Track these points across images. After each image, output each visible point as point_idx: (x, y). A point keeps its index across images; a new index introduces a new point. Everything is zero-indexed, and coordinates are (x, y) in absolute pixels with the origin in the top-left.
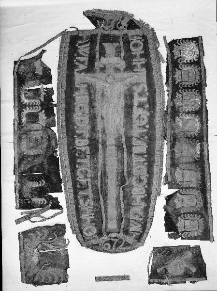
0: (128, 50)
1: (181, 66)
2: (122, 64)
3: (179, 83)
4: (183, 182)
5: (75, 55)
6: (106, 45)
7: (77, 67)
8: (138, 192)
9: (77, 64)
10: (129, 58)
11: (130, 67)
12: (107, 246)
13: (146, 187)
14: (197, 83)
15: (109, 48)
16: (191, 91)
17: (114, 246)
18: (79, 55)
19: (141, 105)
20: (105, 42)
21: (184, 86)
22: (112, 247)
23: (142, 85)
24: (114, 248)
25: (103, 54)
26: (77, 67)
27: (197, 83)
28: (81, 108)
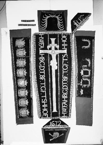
0: (61, 41)
1: (26, 106)
2: (58, 47)
3: (27, 100)
4: (23, 61)
5: (39, 43)
6: (51, 39)
7: (40, 47)
8: (65, 96)
9: (66, 104)
10: (61, 44)
11: (61, 48)
12: (53, 125)
13: (67, 94)
14: (20, 100)
15: (53, 40)
16: (21, 96)
17: (56, 124)
18: (65, 108)
19: (65, 62)
20: (56, 112)
21: (25, 99)
22: (55, 124)
23: (65, 54)
24: (56, 125)
25: (50, 42)
26: (40, 47)
27: (20, 100)
28: (15, 33)
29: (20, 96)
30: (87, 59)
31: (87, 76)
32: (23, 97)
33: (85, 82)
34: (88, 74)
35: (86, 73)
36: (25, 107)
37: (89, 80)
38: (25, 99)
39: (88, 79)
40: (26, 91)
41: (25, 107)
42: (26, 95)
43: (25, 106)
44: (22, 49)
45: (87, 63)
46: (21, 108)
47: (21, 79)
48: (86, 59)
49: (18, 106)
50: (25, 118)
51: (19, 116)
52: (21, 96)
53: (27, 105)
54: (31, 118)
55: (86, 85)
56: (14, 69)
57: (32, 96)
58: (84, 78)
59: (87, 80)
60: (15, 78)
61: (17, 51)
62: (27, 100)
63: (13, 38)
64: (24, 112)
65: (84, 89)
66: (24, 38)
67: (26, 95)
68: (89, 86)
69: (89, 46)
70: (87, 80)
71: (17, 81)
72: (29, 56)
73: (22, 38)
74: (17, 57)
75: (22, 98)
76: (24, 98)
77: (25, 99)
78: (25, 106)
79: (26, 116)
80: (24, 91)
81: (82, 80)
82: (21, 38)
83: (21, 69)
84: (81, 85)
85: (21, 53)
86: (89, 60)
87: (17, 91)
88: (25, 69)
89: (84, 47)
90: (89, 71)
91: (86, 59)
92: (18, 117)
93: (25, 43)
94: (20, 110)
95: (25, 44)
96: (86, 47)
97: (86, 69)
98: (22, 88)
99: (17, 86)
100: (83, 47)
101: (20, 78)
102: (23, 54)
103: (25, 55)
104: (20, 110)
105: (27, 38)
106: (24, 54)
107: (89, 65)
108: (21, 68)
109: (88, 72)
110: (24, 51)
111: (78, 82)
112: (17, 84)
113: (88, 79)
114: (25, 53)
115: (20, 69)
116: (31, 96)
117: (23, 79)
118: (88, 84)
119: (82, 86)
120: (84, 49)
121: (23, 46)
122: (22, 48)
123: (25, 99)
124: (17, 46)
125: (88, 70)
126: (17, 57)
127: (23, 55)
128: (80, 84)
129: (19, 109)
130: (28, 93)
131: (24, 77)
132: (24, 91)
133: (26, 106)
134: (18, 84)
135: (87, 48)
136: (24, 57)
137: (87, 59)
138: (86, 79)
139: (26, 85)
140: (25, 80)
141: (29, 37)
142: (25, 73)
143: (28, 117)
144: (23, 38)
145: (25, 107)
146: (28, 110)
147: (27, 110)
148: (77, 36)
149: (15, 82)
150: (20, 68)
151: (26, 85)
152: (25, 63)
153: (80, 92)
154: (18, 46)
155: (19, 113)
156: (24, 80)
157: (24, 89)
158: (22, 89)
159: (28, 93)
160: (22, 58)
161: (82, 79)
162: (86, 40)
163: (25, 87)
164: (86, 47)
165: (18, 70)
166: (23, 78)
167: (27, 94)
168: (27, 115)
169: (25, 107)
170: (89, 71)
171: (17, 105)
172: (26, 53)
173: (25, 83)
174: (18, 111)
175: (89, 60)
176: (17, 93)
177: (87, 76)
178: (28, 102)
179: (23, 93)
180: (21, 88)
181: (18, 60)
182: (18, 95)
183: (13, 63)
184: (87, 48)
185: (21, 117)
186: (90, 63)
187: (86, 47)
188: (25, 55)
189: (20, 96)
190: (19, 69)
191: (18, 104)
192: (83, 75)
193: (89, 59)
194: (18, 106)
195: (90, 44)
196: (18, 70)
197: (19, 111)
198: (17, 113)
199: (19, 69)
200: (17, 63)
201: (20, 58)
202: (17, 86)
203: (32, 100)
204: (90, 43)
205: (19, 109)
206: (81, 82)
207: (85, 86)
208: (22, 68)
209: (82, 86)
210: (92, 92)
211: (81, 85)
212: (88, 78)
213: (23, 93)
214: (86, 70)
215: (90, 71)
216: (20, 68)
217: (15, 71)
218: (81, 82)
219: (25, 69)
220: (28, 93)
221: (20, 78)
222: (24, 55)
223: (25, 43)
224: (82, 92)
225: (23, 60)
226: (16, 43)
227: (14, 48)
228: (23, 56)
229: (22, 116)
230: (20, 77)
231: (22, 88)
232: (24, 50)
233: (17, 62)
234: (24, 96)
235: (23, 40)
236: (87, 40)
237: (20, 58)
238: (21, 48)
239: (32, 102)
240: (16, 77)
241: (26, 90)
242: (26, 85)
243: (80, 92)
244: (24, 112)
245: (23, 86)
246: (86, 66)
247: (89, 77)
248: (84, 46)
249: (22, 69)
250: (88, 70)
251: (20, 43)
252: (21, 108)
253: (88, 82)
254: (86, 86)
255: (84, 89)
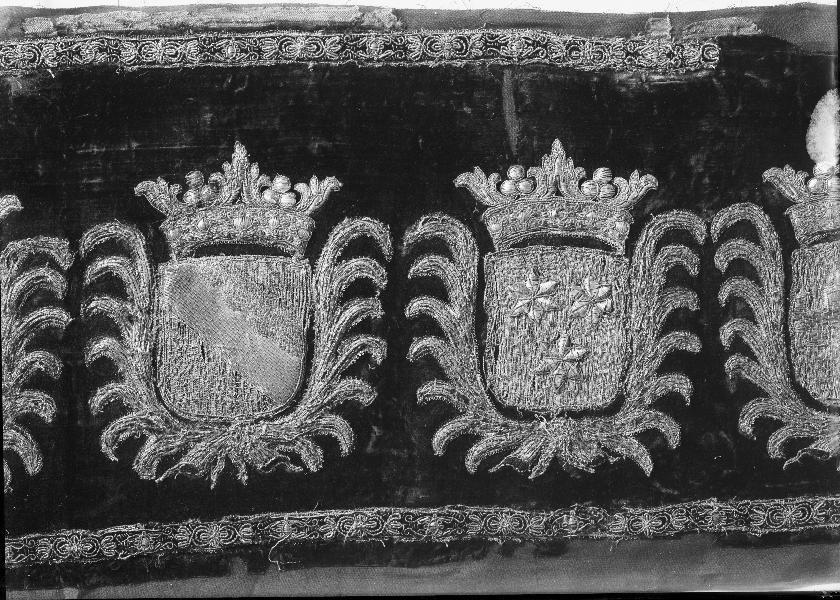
14: (766, 426)
16: (673, 362)
21: (742, 268)
29: (668, 403)
47: (107, 370)
52: (673, 362)
54: (486, 16)
67: (615, 229)
75: (714, 355)
76: (707, 282)
80: (506, 270)
99: (342, 480)
117: (113, 286)
130: (586, 159)
131: (57, 247)
132: (516, 285)
134: (248, 444)
139: (318, 190)
140: (147, 218)
150: (704, 367)
151: (326, 217)
156: (159, 252)
158: (427, 325)
159: (557, 163)
163: (361, 246)
167: (608, 198)
178: (787, 166)
180: (397, 349)
189: (668, 403)
202: (342, 480)
220: (557, 163)
231: (397, 329)
234: (676, 277)
241: (468, 210)
242: (318, 190)
245: (359, 288)
252: (431, 390)
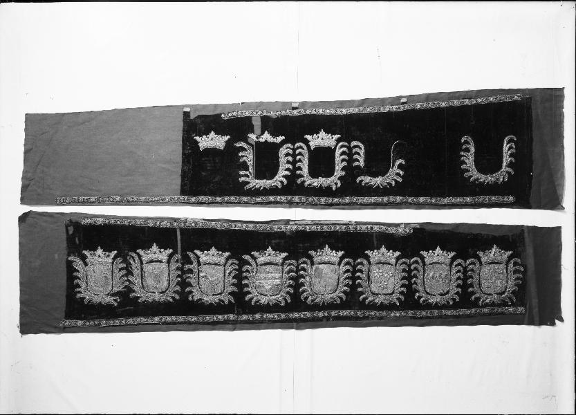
1: (459, 264)
3: (423, 258)
4: (199, 264)
14: (420, 297)
16: (403, 286)
29: (402, 293)
30: (400, 166)
31: (305, 170)
32: (409, 276)
33: (267, 160)
34: (314, 173)
35: (322, 161)
36: (465, 268)
37: (280, 178)
38: (416, 269)
39: (287, 173)
40: (374, 255)
41: (465, 268)
42: (398, 259)
43: (459, 271)
44: (135, 265)
45: (377, 165)
46: (470, 289)
47: (302, 284)
48: (398, 162)
49: (456, 306)
50: (524, 273)
51: (513, 305)
52: (403, 286)
53: (453, 259)
55: (250, 163)
56: (245, 317)
57: (407, 224)
58: (294, 150)
59: (282, 172)
60: (296, 315)
61: (144, 299)
62: (424, 253)
63: (69, 316)
64: (494, 274)
65: (230, 153)
66: (69, 255)
68: (247, 180)
69: (475, 174)
70: (282, 172)
71: (316, 307)
72: (174, 230)
73: (69, 265)
74: (177, 297)
75: (411, 284)
76: (409, 271)
77: (420, 268)
78: (459, 271)
79: (515, 264)
80: (373, 267)
81: (280, 139)
82: (71, 269)
83: (246, 278)
84: (252, 137)
85: (155, 272)
86: (394, 174)
87: (373, 306)
88: (246, 257)
89: (468, 150)
90: (333, 181)
91: (398, 162)
92: (521, 309)
93: (100, 251)
94: (478, 299)
95: (107, 249)
96: (472, 158)
97: (345, 164)
98: (354, 278)
99: (343, 305)
100: (470, 139)
101: (297, 284)
102: (164, 266)
103: (170, 251)
104: (478, 299)
105: (70, 240)
106: (164, 255)
107: (366, 179)
108: (239, 277)
109: (329, 172)
110: (146, 255)
111: (265, 120)
112: (331, 306)
113: (287, 173)
114: (155, 253)
115: (247, 285)
116: (400, 230)
118: (259, 175)
119: (246, 140)
120: (457, 148)
121: (114, 259)
122: (126, 268)
123: (420, 268)
124: (113, 295)
125: (339, 172)
126: (177, 297)
127: (168, 262)
128: (257, 128)
129: (475, 304)
133: (459, 264)
135: (463, 166)
136: (178, 256)
137: (400, 166)
138: (288, 162)
139: (340, 253)
140: (310, 258)
141: (67, 227)
142: (270, 255)
143: (519, 257)
144: (71, 258)
145: (465, 270)
146: (481, 254)
147: (479, 259)
148: (529, 108)
149: (320, 320)
150: (240, 285)
151: (342, 258)
152: (211, 256)
153: (212, 134)
154: (116, 289)
155: (493, 304)
157: (365, 268)
158: (359, 278)
159: (383, 249)
160: (183, 272)
161: (283, 143)
162: (506, 159)
163: (348, 263)
164: (469, 160)
165: (254, 296)
166: (296, 272)
167: (392, 256)
168: (510, 258)
169: (465, 270)
170: (333, 181)
171: (449, 313)
172: (155, 248)
173: (326, 259)
174: (486, 310)
175: (394, 174)
176: (382, 307)
177: (305, 171)
179: (383, 274)
181: (197, 295)
182: (391, 307)
183: (213, 325)
184: (463, 166)
185: (520, 295)
186: (379, 181)
187: (469, 160)
188: (170, 251)
190: (249, 293)
191: (446, 306)
192: (309, 147)
193: (400, 180)
194: (456, 306)
195: (490, 179)
196: (250, 296)
197: (483, 307)
198: (496, 315)
199: (249, 293)
200: (216, 299)
201: (184, 284)
202: (343, 305)
203: (427, 228)
204: (496, 183)
205: (475, 304)
206: (267, 137)
207: (249, 157)
208: (240, 270)
209: (246, 140)
210: (210, 199)
211: (252, 137)
212: (293, 176)
213: (383, 274)
214: (339, 165)
215: (334, 188)
216: (240, 285)
217: (258, 316)
218: (267, 137)
219: (246, 257)
220: (383, 249)
221: (297, 284)
222: (170, 256)
223: (100, 251)
224: (213, 141)
225: (195, 264)
226: (97, 300)
227: (127, 312)
228: (174, 266)
229: (511, 285)
230: (290, 286)
231: (354, 278)
232: (140, 256)
233: (208, 299)
235: (84, 258)
236: (510, 165)
237: (184, 284)
238: (130, 273)
239: (440, 228)
240: (288, 308)
241: (367, 257)
242: (340, 253)
243: (212, 134)
244: (494, 274)
245: (347, 271)
246: (362, 164)
247: (299, 181)
248: (473, 150)
249: (247, 271)
250: (339, 172)
251: (99, 273)
252: (470, 289)
253: (272, 177)
254: (245, 166)
255: (230, 153)
